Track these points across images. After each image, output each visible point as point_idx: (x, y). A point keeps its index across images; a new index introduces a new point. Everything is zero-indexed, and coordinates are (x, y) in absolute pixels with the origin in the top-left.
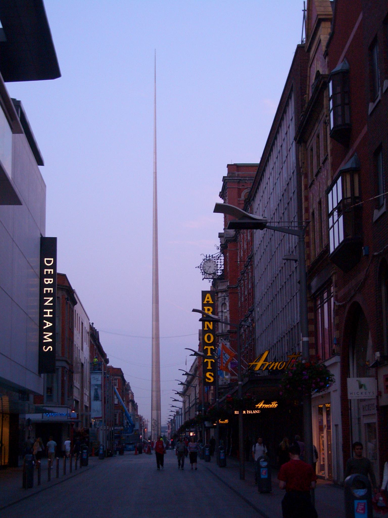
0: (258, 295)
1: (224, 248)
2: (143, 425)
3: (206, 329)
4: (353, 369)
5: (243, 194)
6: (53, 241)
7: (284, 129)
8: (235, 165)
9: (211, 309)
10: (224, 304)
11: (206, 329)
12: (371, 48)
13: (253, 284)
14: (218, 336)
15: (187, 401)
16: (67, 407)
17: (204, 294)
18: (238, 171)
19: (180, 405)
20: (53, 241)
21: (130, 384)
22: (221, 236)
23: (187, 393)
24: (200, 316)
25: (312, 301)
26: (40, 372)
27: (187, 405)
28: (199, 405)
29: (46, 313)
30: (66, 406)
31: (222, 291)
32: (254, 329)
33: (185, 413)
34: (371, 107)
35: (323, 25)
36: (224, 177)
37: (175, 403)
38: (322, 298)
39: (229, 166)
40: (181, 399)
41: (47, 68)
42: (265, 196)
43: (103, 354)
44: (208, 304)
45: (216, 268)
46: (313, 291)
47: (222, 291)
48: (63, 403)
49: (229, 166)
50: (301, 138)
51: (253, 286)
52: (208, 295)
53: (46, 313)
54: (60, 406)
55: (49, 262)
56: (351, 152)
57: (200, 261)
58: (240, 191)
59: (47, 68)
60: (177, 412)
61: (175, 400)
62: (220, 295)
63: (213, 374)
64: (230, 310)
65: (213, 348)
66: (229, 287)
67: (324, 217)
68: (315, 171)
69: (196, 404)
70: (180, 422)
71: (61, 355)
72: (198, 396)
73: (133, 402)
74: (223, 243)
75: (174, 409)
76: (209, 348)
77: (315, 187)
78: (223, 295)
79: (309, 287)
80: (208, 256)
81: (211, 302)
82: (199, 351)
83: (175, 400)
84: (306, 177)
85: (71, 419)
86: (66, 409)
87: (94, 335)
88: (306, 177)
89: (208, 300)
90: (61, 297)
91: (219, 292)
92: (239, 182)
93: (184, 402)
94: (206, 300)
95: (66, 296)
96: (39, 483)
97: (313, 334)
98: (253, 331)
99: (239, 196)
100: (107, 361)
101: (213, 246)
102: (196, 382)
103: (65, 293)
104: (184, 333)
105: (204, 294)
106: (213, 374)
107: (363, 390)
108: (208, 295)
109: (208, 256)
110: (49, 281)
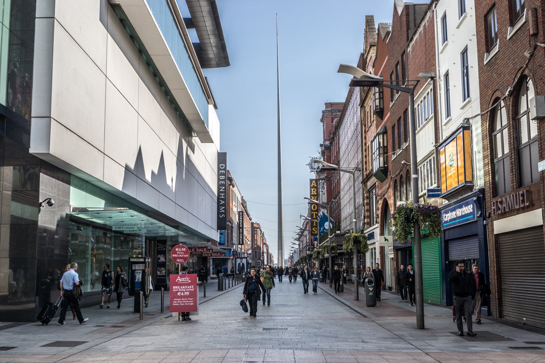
0: (342, 184)
8: (330, 103)
9: (316, 190)
10: (323, 187)
12: (396, 66)
13: (340, 177)
15: (301, 244)
17: (311, 181)
19: (297, 247)
22: (321, 145)
23: (301, 239)
24: (307, 201)
26: (218, 229)
27: (301, 246)
29: (221, 196)
31: (322, 179)
32: (340, 203)
33: (300, 251)
34: (391, 104)
35: (373, 48)
37: (294, 246)
38: (373, 192)
40: (297, 243)
42: (346, 129)
46: (368, 188)
49: (325, 104)
51: (340, 179)
52: (314, 181)
53: (221, 196)
55: (222, 166)
57: (308, 161)
58: (332, 120)
60: (295, 251)
61: (294, 244)
62: (321, 181)
64: (327, 191)
68: (369, 124)
69: (307, 246)
70: (296, 259)
72: (308, 241)
75: (292, 249)
76: (314, 213)
81: (316, 186)
83: (294, 244)
84: (365, 126)
88: (365, 126)
93: (299, 245)
96: (225, 289)
98: (339, 205)
99: (332, 122)
101: (306, 213)
102: (306, 233)
105: (311, 181)
107: (387, 242)
108: (314, 181)
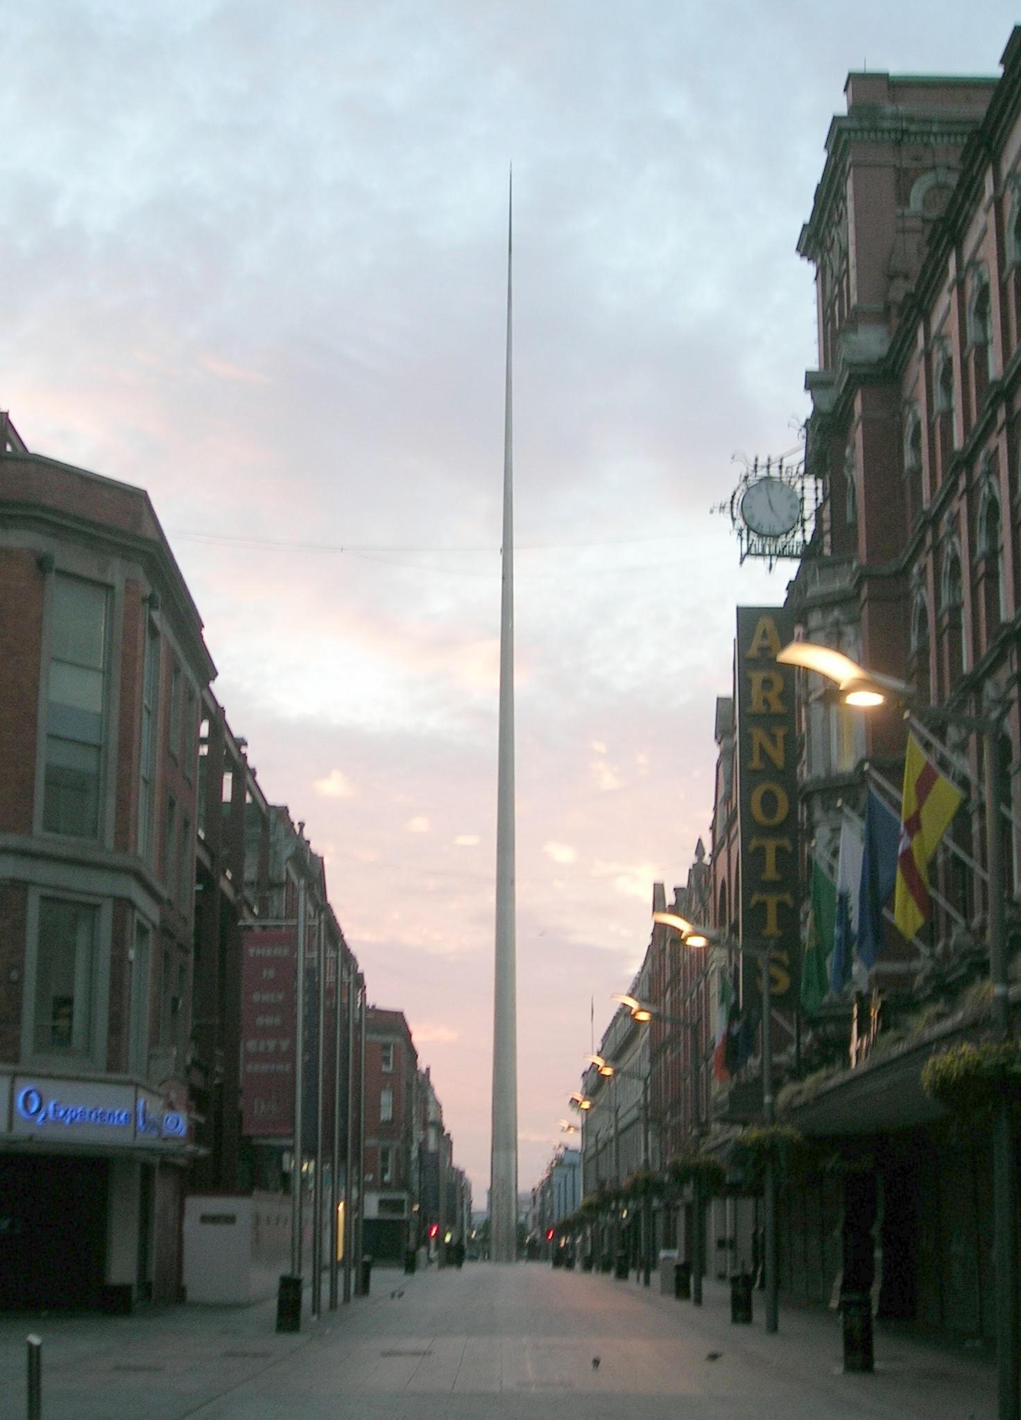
2: (457, 1187)
3: (756, 763)
5: (917, 194)
11: (756, 763)
14: (808, 798)
16: (137, 1085)
18: (893, 100)
21: (433, 1079)
30: (127, 1077)
36: (836, 119)
45: (796, 513)
48: (114, 1064)
54: (102, 1075)
58: (904, 180)
63: (784, 958)
65: (790, 849)
66: (863, 577)
71: (110, 843)
73: (440, 1127)
74: (827, 407)
78: (830, 619)
80: (762, 461)
85: (166, 1139)
86: (130, 1091)
89: (766, 643)
90: (119, 587)
91: (812, 608)
92: (900, 138)
94: (757, 642)
95: (147, 590)
99: (903, 199)
103: (139, 573)
106: (784, 958)
109: (762, 461)
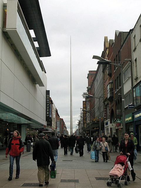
0: (95, 103)
1: (88, 91)
4: (113, 122)
6: (49, 91)
7: (100, 69)
10: (88, 104)
20: (49, 91)
22: (87, 88)
25: (106, 106)
28: (83, 128)
31: (88, 101)
34: (115, 71)
39: (94, 56)
40: (78, 126)
41: (48, 54)
43: (58, 115)
44: (84, 107)
47: (88, 101)
50: (103, 72)
51: (94, 101)
55: (48, 96)
56: (111, 79)
57: (82, 94)
58: (92, 77)
59: (48, 54)
67: (114, 83)
73: (65, 127)
75: (76, 129)
77: (106, 83)
79: (105, 104)
82: (101, 57)
84: (104, 80)
87: (57, 111)
88: (104, 80)
93: (79, 127)
97: (106, 113)
100: (59, 117)
104: (77, 118)
110: (48, 100)
